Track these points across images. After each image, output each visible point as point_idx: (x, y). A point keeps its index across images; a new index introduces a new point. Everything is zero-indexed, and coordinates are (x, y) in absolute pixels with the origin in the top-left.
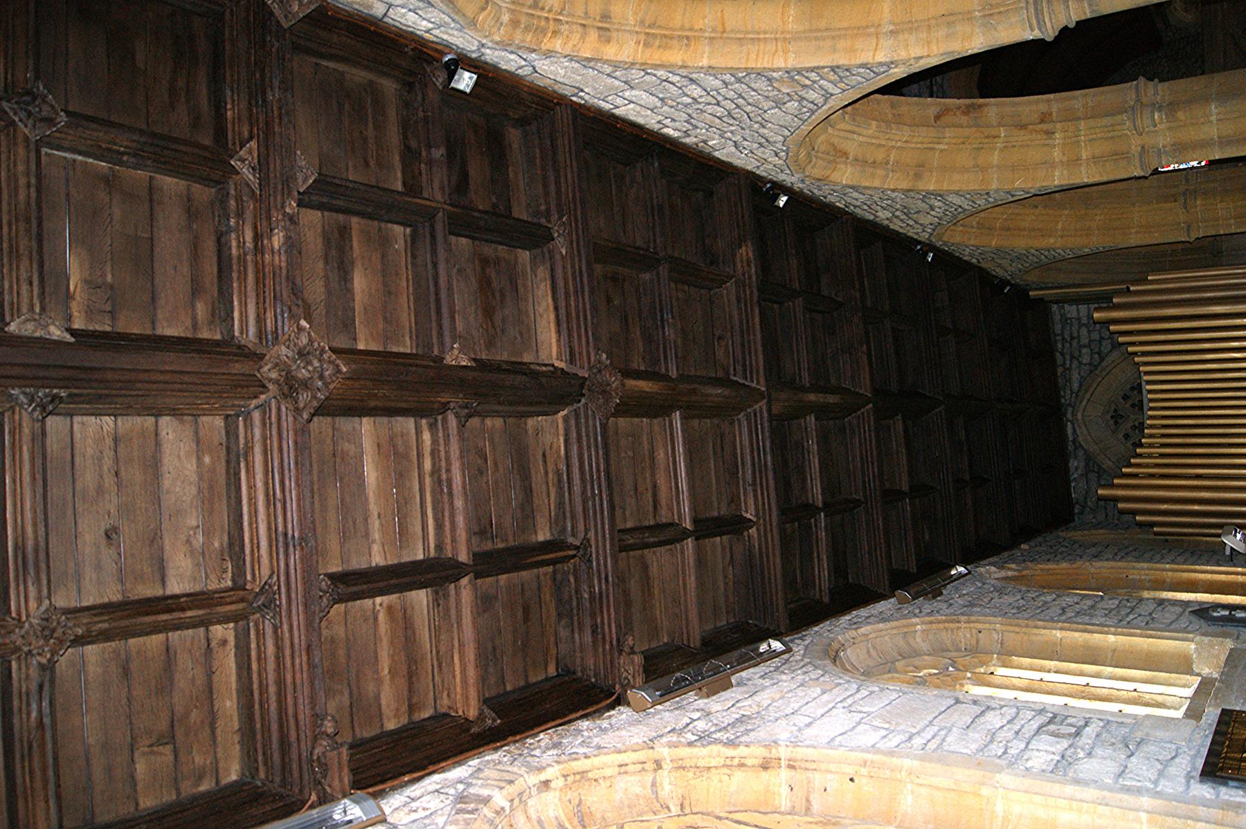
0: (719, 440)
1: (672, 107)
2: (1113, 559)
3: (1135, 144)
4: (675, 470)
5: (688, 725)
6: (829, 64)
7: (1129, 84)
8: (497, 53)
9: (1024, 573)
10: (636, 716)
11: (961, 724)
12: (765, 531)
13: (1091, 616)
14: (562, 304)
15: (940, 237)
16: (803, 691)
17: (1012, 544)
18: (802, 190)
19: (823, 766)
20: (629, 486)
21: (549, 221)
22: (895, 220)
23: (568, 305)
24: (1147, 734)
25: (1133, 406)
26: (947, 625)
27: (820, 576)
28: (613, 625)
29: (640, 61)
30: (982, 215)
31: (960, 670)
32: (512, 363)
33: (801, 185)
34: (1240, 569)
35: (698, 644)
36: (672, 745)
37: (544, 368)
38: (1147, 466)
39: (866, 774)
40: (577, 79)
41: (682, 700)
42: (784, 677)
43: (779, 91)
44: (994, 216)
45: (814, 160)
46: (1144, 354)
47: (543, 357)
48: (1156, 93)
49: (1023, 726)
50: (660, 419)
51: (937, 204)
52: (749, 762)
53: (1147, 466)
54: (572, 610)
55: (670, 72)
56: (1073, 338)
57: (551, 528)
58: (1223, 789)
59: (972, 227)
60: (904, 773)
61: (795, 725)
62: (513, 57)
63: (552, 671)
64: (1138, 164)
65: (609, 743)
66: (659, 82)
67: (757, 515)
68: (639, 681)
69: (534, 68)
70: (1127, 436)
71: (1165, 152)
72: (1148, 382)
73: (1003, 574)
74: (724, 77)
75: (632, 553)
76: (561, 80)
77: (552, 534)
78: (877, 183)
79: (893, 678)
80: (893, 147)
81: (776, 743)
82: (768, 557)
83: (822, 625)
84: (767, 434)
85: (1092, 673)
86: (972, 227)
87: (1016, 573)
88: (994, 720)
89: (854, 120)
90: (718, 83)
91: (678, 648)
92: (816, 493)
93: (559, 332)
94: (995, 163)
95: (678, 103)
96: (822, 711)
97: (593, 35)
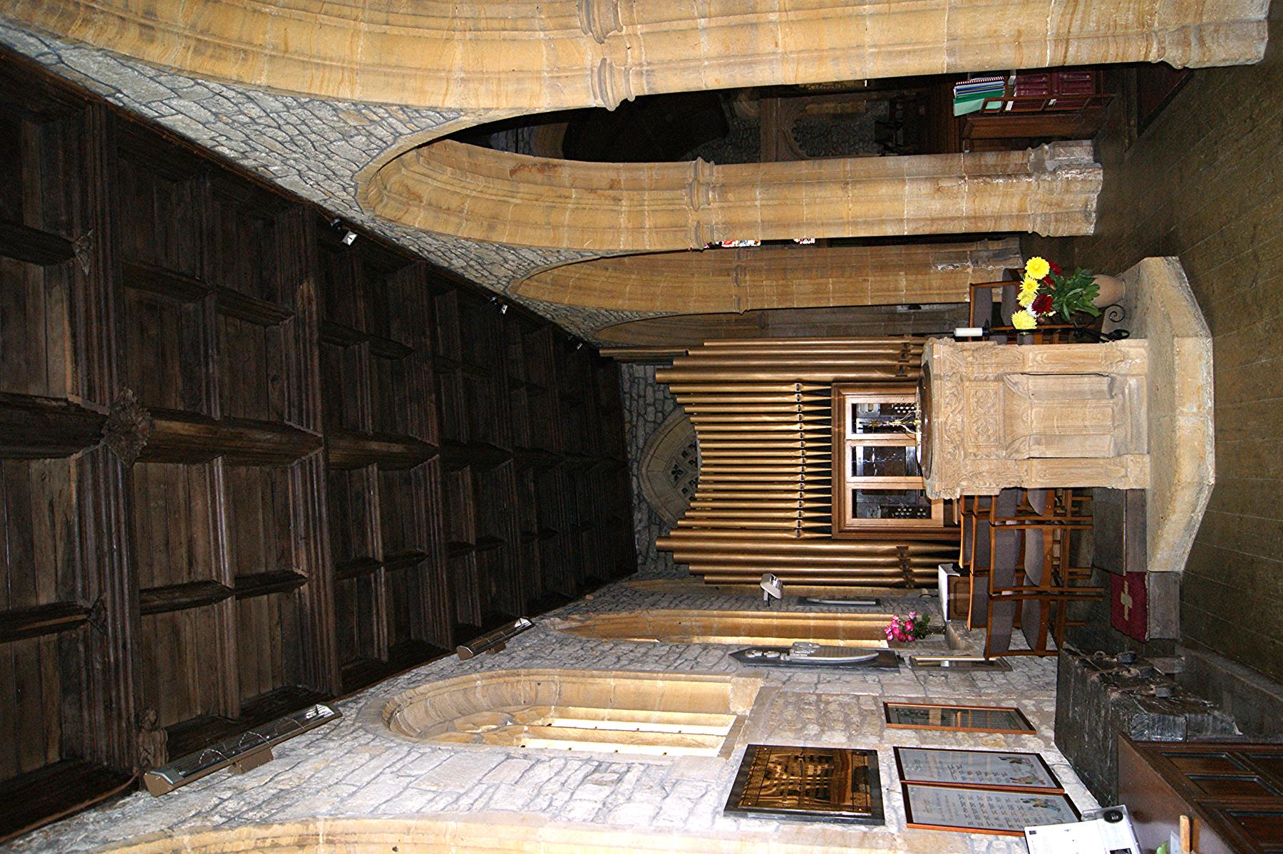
0: (269, 491)
1: (227, 124)
2: (668, 607)
3: (692, 219)
4: (215, 521)
5: (216, 806)
6: (398, 102)
7: (689, 163)
8: (11, 33)
9: (588, 623)
10: (155, 801)
11: (510, 780)
12: (318, 587)
13: (644, 663)
14: (81, 330)
15: (515, 289)
16: (350, 758)
17: (579, 594)
18: (372, 229)
19: (364, 838)
20: (158, 538)
21: (71, 235)
22: (469, 269)
23: (88, 335)
24: (682, 775)
25: (691, 462)
26: (507, 679)
27: (379, 634)
28: (131, 699)
29: (188, 68)
30: (556, 272)
31: (517, 724)
32: (13, 395)
33: (372, 225)
34: (775, 613)
35: (237, 714)
36: (192, 832)
37: (54, 403)
38: (701, 519)
39: (410, 841)
40: (114, 79)
41: (213, 778)
42: (331, 744)
43: (345, 122)
44: (567, 274)
45: (385, 199)
46: (700, 414)
47: (55, 391)
48: (711, 174)
49: (569, 777)
50: (199, 466)
51: (511, 257)
52: (283, 841)
53: (701, 519)
54: (80, 684)
55: (223, 85)
56: (639, 396)
57: (56, 590)
58: (743, 821)
59: (546, 283)
60: (448, 837)
61: (337, 796)
62: (32, 40)
63: (54, 756)
64: (693, 238)
65: (120, 836)
66: (211, 94)
67: (309, 571)
68: (161, 760)
69: (60, 57)
70: (685, 491)
71: (717, 229)
72: (703, 441)
73: (567, 625)
74: (285, 100)
75: (159, 616)
76: (94, 76)
77: (58, 596)
78: (450, 231)
79: (450, 737)
80: (468, 196)
81: (314, 817)
82: (320, 615)
83: (378, 686)
84: (323, 484)
85: (642, 719)
86: (546, 283)
87: (578, 624)
88: (542, 772)
89: (429, 163)
90: (278, 106)
91: (213, 720)
92: (376, 547)
93: (76, 362)
94: (566, 223)
95: (234, 121)
96: (367, 779)
97: (133, 31)
